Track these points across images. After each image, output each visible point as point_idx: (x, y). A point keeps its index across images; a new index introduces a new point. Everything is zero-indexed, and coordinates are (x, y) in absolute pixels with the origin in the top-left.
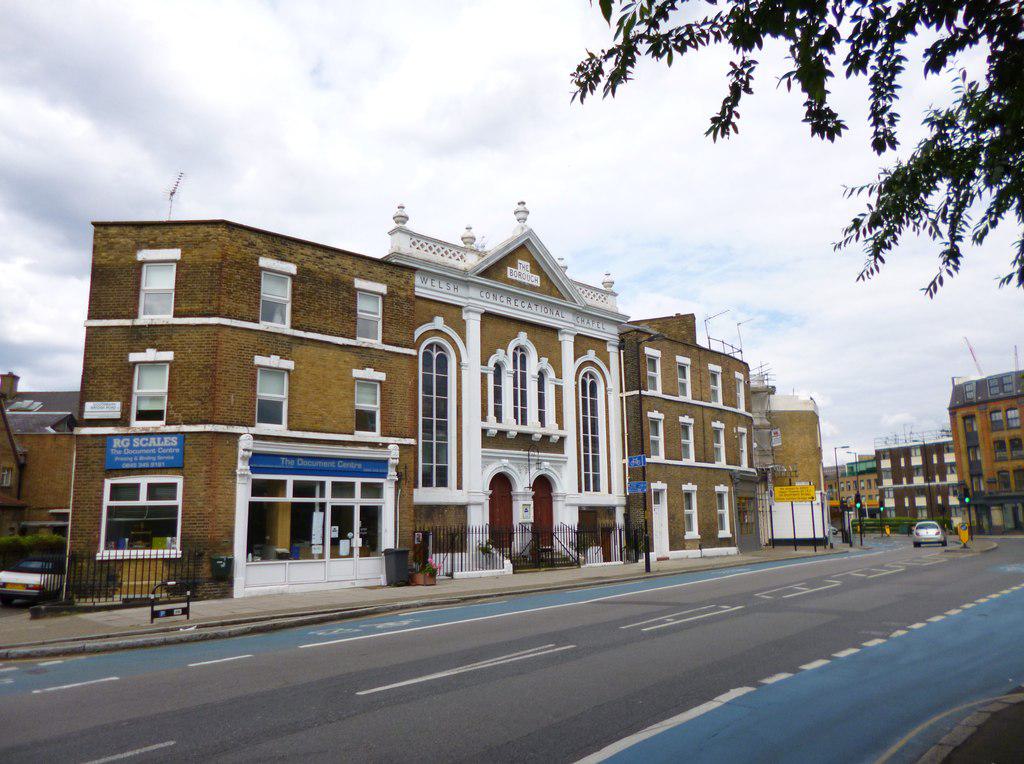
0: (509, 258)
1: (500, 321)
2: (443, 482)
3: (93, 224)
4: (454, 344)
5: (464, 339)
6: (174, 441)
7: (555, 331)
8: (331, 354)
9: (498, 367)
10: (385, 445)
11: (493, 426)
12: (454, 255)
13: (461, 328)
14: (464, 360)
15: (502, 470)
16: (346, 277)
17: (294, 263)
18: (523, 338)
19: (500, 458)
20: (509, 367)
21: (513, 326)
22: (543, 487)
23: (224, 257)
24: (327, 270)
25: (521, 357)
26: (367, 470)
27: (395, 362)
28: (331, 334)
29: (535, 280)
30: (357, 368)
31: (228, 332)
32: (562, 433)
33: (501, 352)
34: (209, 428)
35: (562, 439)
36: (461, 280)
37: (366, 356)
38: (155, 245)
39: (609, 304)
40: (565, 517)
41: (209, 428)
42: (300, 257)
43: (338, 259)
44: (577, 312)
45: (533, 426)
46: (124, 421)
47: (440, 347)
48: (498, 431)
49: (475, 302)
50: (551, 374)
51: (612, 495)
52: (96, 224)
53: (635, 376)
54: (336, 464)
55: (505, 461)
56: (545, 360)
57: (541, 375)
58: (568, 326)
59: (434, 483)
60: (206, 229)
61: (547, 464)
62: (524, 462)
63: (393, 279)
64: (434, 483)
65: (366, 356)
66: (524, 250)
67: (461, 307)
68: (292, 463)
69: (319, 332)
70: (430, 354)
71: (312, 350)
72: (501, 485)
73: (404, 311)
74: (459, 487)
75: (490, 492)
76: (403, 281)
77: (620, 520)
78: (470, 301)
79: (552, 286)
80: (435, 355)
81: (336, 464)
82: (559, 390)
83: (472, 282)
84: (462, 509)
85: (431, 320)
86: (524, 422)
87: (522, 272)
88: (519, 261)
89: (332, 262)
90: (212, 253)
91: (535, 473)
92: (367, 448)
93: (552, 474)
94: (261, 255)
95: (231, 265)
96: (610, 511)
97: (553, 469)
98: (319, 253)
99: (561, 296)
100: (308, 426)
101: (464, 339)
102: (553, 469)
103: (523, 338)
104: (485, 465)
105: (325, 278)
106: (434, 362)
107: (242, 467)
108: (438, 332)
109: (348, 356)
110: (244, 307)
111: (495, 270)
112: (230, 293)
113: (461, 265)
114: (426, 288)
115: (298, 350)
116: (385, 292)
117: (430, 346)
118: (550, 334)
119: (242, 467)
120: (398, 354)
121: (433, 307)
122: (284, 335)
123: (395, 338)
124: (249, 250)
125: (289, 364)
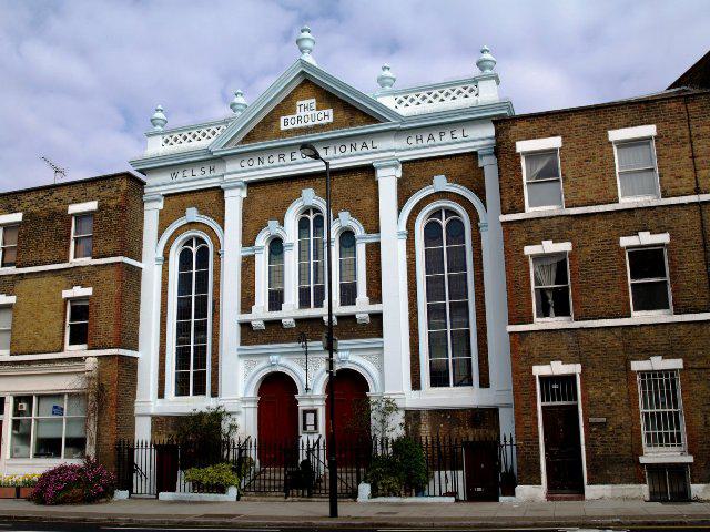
1: (268, 187)
4: (210, 232)
8: (44, 281)
9: (276, 245)
11: (261, 312)
15: (268, 371)
18: (309, 197)
19: (269, 354)
20: (290, 233)
22: (348, 389)
27: (102, 274)
29: (327, 115)
30: (66, 288)
32: (376, 308)
33: (273, 224)
35: (377, 318)
36: (213, 160)
42: (25, 205)
44: (397, 132)
47: (449, 212)
49: (234, 178)
50: (359, 231)
55: (284, 359)
57: (347, 237)
58: (387, 156)
59: (451, 383)
61: (352, 356)
63: (106, 193)
64: (451, 383)
70: (439, 224)
72: (277, 390)
74: (485, 383)
75: (297, 397)
79: (353, 112)
80: (194, 250)
82: (374, 251)
83: (226, 155)
88: (299, 103)
91: (262, 368)
99: (376, 121)
100: (24, 349)
106: (444, 231)
108: (192, 224)
109: (60, 280)
111: (263, 130)
114: (179, 182)
117: (437, 213)
118: (360, 176)
125: (12, 299)
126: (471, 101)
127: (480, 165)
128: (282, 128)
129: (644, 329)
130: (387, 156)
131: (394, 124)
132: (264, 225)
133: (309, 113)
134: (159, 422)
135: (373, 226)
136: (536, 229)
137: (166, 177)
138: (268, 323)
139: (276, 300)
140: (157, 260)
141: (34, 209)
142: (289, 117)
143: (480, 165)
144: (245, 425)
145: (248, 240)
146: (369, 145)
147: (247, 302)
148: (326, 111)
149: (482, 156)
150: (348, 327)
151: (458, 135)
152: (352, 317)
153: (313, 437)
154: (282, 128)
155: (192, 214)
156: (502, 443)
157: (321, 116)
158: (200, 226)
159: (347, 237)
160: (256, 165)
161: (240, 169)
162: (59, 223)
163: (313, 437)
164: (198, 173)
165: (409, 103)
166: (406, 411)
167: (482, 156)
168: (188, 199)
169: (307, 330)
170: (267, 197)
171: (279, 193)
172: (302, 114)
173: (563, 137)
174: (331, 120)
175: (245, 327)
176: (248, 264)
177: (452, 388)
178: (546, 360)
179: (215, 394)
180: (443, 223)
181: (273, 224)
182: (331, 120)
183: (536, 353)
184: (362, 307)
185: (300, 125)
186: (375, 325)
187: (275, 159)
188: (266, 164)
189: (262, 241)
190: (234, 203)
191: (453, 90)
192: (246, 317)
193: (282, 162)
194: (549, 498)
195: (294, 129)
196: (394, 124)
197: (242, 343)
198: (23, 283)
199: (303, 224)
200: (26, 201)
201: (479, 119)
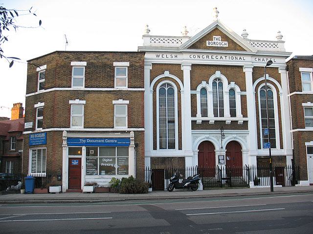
0: (209, 36)
2: (172, 146)
3: (28, 61)
5: (280, 82)
6: (44, 135)
7: (241, 67)
9: (204, 90)
10: (129, 132)
11: (199, 118)
12: (260, 45)
13: (180, 75)
14: (281, 91)
16: (109, 63)
17: (86, 61)
18: (218, 74)
20: (210, 88)
21: (212, 69)
22: (234, 148)
23: (57, 65)
24: (100, 61)
25: (218, 83)
27: (134, 95)
28: (102, 87)
29: (225, 44)
31: (58, 92)
32: (245, 119)
33: (204, 83)
34: (52, 129)
35: (246, 123)
37: (120, 95)
38: (39, 66)
39: (280, 48)
40: (249, 160)
41: (52, 129)
43: (105, 56)
45: (227, 118)
46: (33, 129)
47: (169, 85)
48: (202, 121)
49: (187, 61)
51: (285, 149)
52: (28, 61)
53: (295, 83)
54: (105, 141)
56: (233, 83)
57: (232, 91)
58: (248, 65)
60: (52, 55)
62: (219, 135)
63: (133, 59)
65: (120, 95)
66: (216, 30)
67: (180, 64)
68: (84, 141)
69: (97, 87)
71: (94, 95)
72: (206, 149)
73: (136, 75)
74: (282, 147)
76: (138, 58)
77: (289, 163)
78: (184, 61)
79: (234, 46)
81: (105, 141)
82: (244, 99)
84: (182, 159)
86: (235, 116)
87: (217, 41)
89: (102, 57)
90: (54, 63)
92: (120, 133)
93: (240, 140)
94: (72, 61)
95: (60, 67)
96: (283, 158)
97: (239, 138)
98: (97, 55)
100: (92, 126)
101: (280, 82)
102: (239, 138)
103: (218, 74)
104: (194, 139)
105: (100, 65)
107: (65, 143)
108: (167, 78)
109: (110, 96)
110: (65, 82)
111: (198, 45)
112: (59, 78)
113: (179, 45)
115: (87, 96)
116: (129, 65)
117: (164, 85)
118: (237, 69)
119: (65, 143)
120: (136, 91)
121: (164, 67)
122: (81, 91)
123: (133, 84)
124: (67, 60)
126: (275, 49)
127: (244, 71)
128: (207, 45)
130: (248, 65)
133: (217, 41)
134: (154, 160)
135: (243, 89)
136: (306, 98)
137: (153, 56)
139: (205, 113)
140: (151, 91)
141: (92, 61)
142: (210, 42)
143: (244, 71)
144: (192, 163)
145: (193, 88)
147: (194, 114)
148: (225, 42)
149: (245, 68)
150: (234, 125)
151: (165, 56)
153: (221, 165)
154: (207, 45)
156: (145, 169)
159: (232, 91)
162: (108, 69)
163: (221, 165)
166: (151, 158)
167: (245, 68)
169: (220, 125)
170: (200, 72)
171: (206, 71)
172: (216, 41)
174: (227, 46)
175: (194, 122)
176: (193, 97)
177: (167, 149)
178: (309, 141)
179: (180, 148)
181: (204, 83)
182: (227, 46)
183: (306, 138)
184: (239, 117)
185: (215, 46)
186: (245, 125)
189: (199, 88)
190: (187, 71)
192: (194, 119)
198: (89, 95)
199: (214, 83)
200: (88, 57)
201: (154, 51)
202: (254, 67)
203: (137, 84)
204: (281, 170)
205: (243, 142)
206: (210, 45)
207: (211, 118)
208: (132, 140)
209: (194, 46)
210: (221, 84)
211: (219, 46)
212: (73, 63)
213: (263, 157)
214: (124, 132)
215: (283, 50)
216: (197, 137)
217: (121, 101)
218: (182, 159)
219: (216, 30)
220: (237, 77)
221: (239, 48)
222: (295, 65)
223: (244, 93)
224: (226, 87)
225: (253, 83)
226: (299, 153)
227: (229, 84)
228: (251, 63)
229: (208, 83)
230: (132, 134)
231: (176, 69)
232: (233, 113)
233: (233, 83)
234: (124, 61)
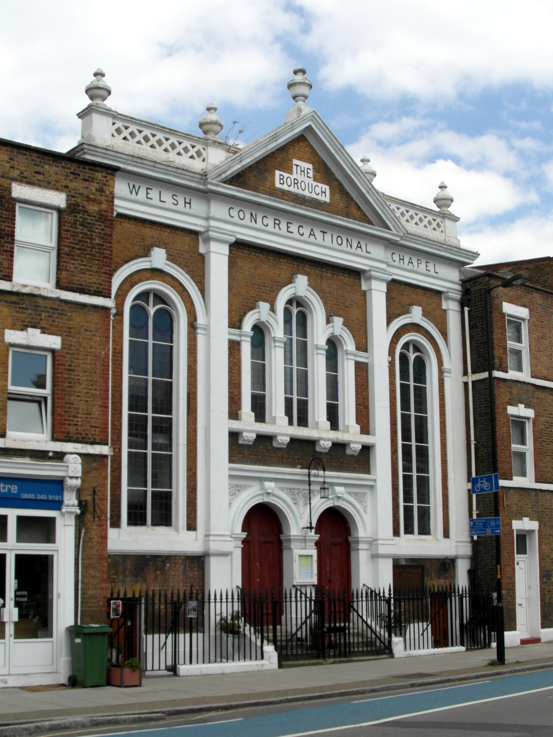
0: (278, 158)
2: (164, 518)
9: (259, 330)
10: (60, 456)
11: (249, 426)
13: (198, 269)
18: (301, 285)
21: (285, 266)
22: (335, 528)
26: (25, 496)
27: (78, 319)
29: (322, 192)
30: (13, 327)
32: (367, 439)
33: (264, 306)
35: (367, 449)
40: (373, 574)
44: (390, 244)
45: (319, 430)
47: (160, 298)
48: (292, 439)
50: (349, 344)
51: (449, 541)
53: (484, 350)
55: (274, 485)
56: (338, 321)
57: (333, 345)
61: (341, 489)
63: (78, 185)
72: (264, 523)
76: (94, 187)
77: (462, 580)
82: (362, 370)
84: (197, 563)
85: (146, 253)
86: (303, 421)
87: (299, 178)
92: (27, 460)
96: (446, 565)
101: (445, 334)
103: (301, 285)
108: (156, 273)
111: (254, 176)
113: (197, 165)
117: (144, 296)
118: (347, 279)
120: (84, 306)
121: (148, 232)
123: (78, 279)
129: (512, 491)
131: (394, 235)
132: (252, 307)
133: (299, 178)
135: (363, 346)
138: (294, 441)
143: (444, 307)
144: (225, 578)
145: (235, 322)
146: (259, 219)
147: (234, 413)
150: (341, 458)
151: (154, 194)
152: (312, 443)
155: (158, 258)
157: (318, 190)
158: (136, 278)
160: (181, 206)
161: (227, 217)
164: (167, 197)
165: (129, 137)
168: (165, 234)
169: (303, 453)
172: (300, 178)
173: (530, 310)
174: (327, 199)
175: (234, 436)
176: (234, 347)
179: (191, 526)
180: (152, 310)
181: (264, 306)
182: (327, 199)
184: (351, 434)
186: (363, 460)
187: (270, 221)
188: (259, 225)
191: (154, 136)
192: (236, 425)
193: (277, 230)
194: (280, 666)
195: (290, 193)
196: (394, 235)
197: (231, 461)
202: (394, 281)
203: (92, 279)
204: (442, 597)
205: (358, 512)
206: (285, 187)
207: (281, 428)
208: (71, 488)
209: (238, 179)
210: (303, 319)
211: (306, 193)
212: (19, 191)
213: (404, 563)
214: (40, 455)
215: (453, 242)
216: (244, 488)
217: (35, 337)
218: (197, 563)
219: (303, 144)
220: (347, 304)
221: (354, 211)
222: (483, 289)
223: (362, 358)
224: (320, 330)
225: (389, 322)
226: (490, 555)
227: (328, 321)
228: (384, 266)
229: (273, 309)
230: (73, 467)
231: (186, 246)
232: (300, 413)
233: (338, 321)
234: (47, 185)
